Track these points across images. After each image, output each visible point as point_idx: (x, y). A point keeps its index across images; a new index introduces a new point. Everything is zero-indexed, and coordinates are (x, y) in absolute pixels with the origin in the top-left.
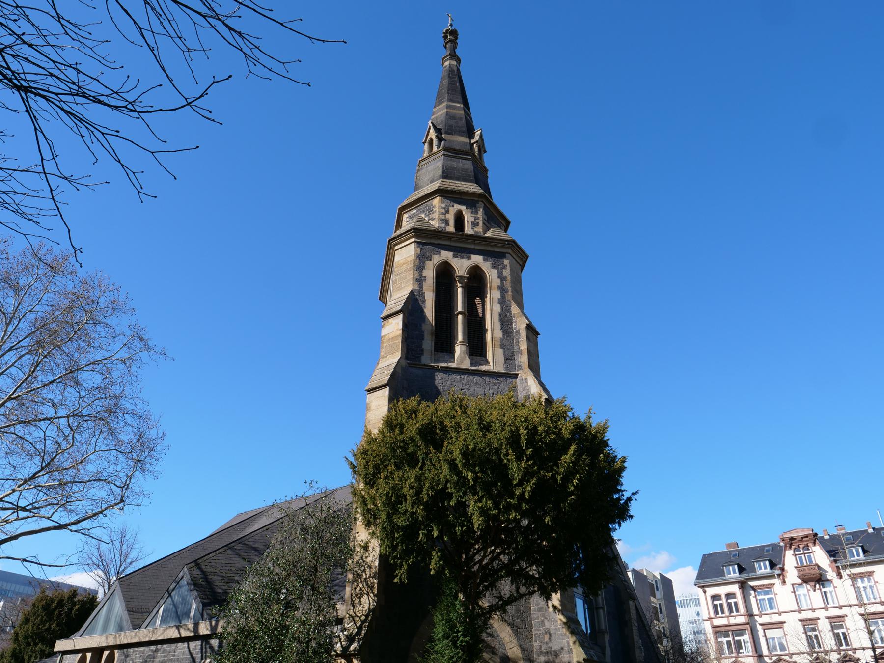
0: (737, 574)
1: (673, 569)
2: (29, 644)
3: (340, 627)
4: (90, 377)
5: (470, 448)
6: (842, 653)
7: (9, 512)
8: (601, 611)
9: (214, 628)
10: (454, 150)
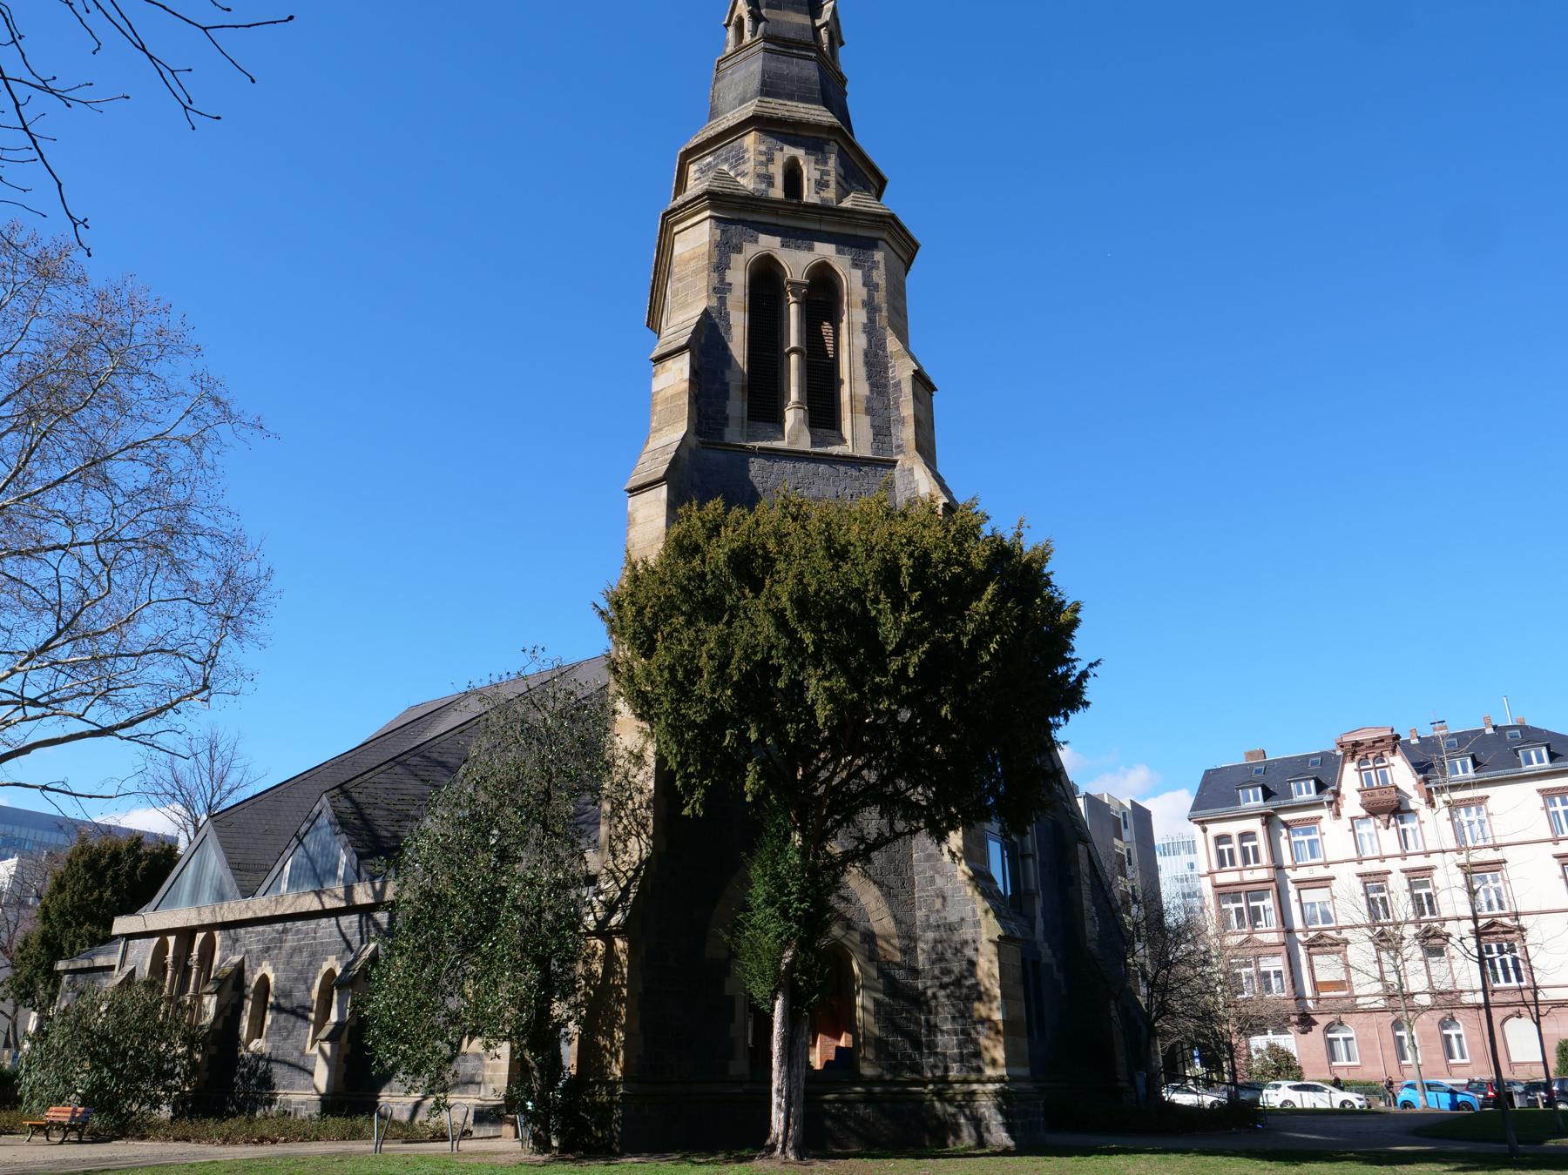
0: (1261, 802)
1: (1155, 793)
2: (68, 925)
3: (591, 889)
4: (129, 471)
5: (811, 589)
6: (1423, 925)
7: (10, 708)
8: (1030, 861)
9: (379, 894)
10: (784, 39)
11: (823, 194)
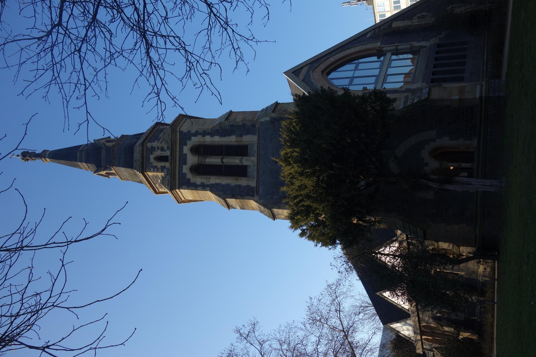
11: (166, 149)
